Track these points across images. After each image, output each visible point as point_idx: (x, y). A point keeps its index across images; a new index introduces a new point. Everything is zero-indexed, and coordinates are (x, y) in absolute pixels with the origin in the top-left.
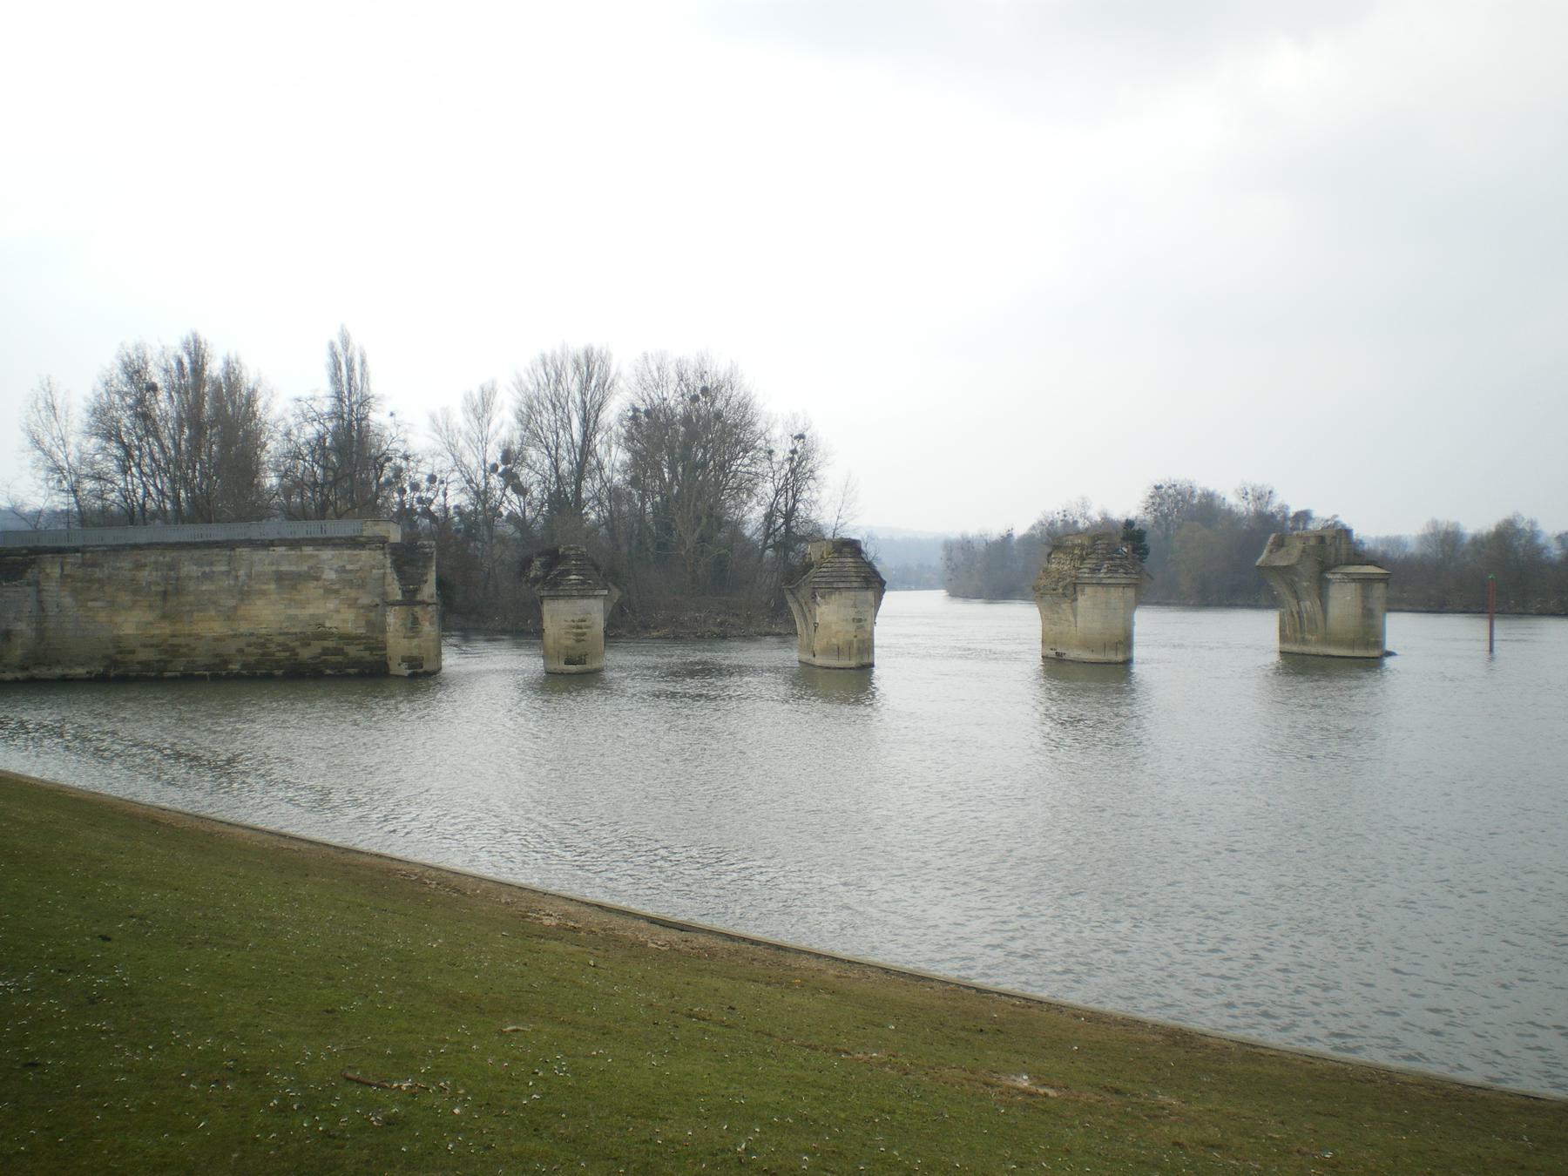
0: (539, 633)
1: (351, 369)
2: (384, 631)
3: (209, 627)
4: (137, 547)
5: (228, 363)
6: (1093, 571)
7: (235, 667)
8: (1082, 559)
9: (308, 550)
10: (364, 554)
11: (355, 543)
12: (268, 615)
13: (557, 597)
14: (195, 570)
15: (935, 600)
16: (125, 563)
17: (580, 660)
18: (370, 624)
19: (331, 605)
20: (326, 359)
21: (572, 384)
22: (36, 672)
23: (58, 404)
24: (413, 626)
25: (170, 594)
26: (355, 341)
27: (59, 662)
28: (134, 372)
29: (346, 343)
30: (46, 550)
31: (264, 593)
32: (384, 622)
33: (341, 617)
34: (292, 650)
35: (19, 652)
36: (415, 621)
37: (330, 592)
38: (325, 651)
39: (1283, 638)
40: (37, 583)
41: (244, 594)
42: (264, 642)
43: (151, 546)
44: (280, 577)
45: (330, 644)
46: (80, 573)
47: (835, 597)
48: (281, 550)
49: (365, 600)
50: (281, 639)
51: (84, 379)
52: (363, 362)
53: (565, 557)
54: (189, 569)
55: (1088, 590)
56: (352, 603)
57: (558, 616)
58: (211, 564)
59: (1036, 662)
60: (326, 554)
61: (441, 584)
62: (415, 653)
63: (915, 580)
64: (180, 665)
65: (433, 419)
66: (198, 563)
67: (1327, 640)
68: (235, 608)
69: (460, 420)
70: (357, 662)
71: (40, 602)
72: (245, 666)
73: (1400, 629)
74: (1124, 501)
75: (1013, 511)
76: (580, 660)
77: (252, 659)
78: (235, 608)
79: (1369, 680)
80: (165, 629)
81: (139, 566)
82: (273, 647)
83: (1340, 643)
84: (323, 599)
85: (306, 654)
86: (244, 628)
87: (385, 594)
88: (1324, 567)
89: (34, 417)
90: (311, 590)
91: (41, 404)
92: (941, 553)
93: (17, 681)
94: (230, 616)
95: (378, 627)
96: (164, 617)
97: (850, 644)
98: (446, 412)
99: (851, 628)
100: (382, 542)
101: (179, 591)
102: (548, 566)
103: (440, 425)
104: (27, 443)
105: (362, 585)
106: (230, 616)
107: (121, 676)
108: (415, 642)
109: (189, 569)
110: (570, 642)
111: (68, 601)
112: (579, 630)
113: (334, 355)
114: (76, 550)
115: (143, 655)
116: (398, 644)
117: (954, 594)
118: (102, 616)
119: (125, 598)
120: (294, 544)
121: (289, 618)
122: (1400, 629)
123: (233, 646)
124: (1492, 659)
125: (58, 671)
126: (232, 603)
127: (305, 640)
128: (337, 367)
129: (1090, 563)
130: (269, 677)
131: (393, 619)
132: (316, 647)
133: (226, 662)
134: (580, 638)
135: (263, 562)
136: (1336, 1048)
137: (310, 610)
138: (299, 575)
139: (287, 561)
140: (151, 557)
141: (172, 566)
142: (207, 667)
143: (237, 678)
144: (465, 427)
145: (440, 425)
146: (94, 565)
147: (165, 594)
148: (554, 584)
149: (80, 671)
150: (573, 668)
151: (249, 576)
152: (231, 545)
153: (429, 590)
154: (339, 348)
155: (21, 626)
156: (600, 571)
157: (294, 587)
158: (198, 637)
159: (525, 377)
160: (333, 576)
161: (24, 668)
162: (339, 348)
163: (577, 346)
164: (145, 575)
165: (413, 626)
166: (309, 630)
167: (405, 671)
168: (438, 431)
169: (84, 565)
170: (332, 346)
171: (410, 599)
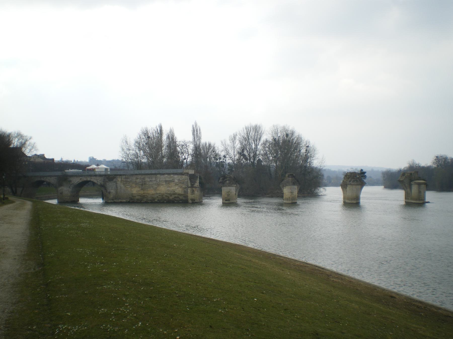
0: (221, 194)
1: (197, 131)
2: (187, 193)
3: (151, 192)
4: (136, 174)
5: (171, 130)
6: (350, 181)
7: (156, 200)
8: (348, 178)
9: (172, 175)
10: (184, 176)
11: (182, 174)
12: (163, 189)
13: (224, 186)
14: (148, 180)
15: (380, 189)
16: (134, 178)
17: (229, 200)
18: (185, 192)
19: (176, 187)
20: (191, 129)
21: (252, 134)
22: (115, 201)
23: (128, 141)
24: (193, 192)
25: (143, 185)
26: (198, 124)
27: (120, 199)
28: (146, 133)
29: (196, 125)
30: (118, 175)
31: (162, 185)
32: (188, 191)
33: (178, 190)
34: (168, 197)
35: (112, 196)
36: (193, 191)
37: (176, 184)
38: (175, 197)
39: (406, 198)
40: (116, 182)
41: (158, 185)
42: (162, 195)
43: (139, 174)
44: (166, 181)
45: (176, 196)
46: (125, 180)
47: (287, 187)
48: (166, 175)
49: (184, 186)
50: (166, 195)
51: (134, 135)
52: (200, 130)
53: (227, 177)
54: (147, 179)
55: (349, 186)
56: (181, 187)
57: (225, 190)
58: (152, 178)
59: (342, 203)
60: (176, 176)
61: (200, 183)
62: (193, 198)
63: (374, 183)
64: (145, 200)
65: (222, 142)
66: (149, 178)
67: (412, 199)
68: (156, 188)
69: (228, 142)
70: (181, 200)
71: (116, 186)
72: (158, 200)
73: (430, 195)
74: (426, 160)
75: (399, 163)
76: (229, 200)
77: (160, 199)
78: (156, 188)
79: (421, 209)
80: (142, 192)
81: (137, 179)
82: (164, 196)
83: (414, 199)
84: (174, 185)
85: (171, 198)
86: (158, 192)
87: (188, 185)
88: (411, 180)
89: (123, 144)
90: (172, 184)
91: (124, 141)
92: (343, 177)
93: (111, 202)
94: (155, 189)
95: (186, 192)
96: (142, 189)
97: (290, 198)
98: (225, 140)
99: (290, 194)
100: (187, 174)
101: (145, 184)
102: (223, 179)
103: (223, 143)
104: (121, 150)
105: (183, 183)
106: (155, 189)
107: (132, 201)
108: (193, 196)
109: (147, 179)
110: (226, 196)
111: (122, 186)
112: (228, 194)
113: (193, 128)
114: (124, 175)
115: (137, 197)
116: (190, 196)
117: (386, 187)
118: (129, 189)
119: (134, 185)
120: (169, 174)
121: (168, 190)
122: (430, 195)
123: (156, 196)
124: (433, 203)
125: (120, 201)
126: (156, 187)
127: (171, 195)
128: (194, 131)
129: (350, 179)
130: (163, 203)
131: (189, 190)
132: (173, 197)
133: (154, 199)
134: (228, 195)
135: (163, 178)
136: (417, 296)
137: (172, 188)
138: (170, 181)
139: (166, 177)
140: (140, 176)
141: (144, 179)
142: (151, 200)
143: (157, 202)
144: (230, 144)
145: (223, 143)
146: (128, 178)
147: (142, 185)
148: (223, 183)
149: (125, 201)
150: (227, 202)
151: (160, 181)
152: (156, 174)
153: (197, 184)
154: (194, 126)
155: (112, 191)
156: (236, 181)
157: (169, 183)
158: (149, 194)
159: (241, 132)
160: (177, 181)
161: (113, 200)
162: (194, 126)
163: (254, 124)
164: (138, 181)
165: (193, 192)
166: (172, 193)
167: (190, 201)
168: (223, 145)
169: (126, 178)
170: (193, 126)
171: (192, 186)
